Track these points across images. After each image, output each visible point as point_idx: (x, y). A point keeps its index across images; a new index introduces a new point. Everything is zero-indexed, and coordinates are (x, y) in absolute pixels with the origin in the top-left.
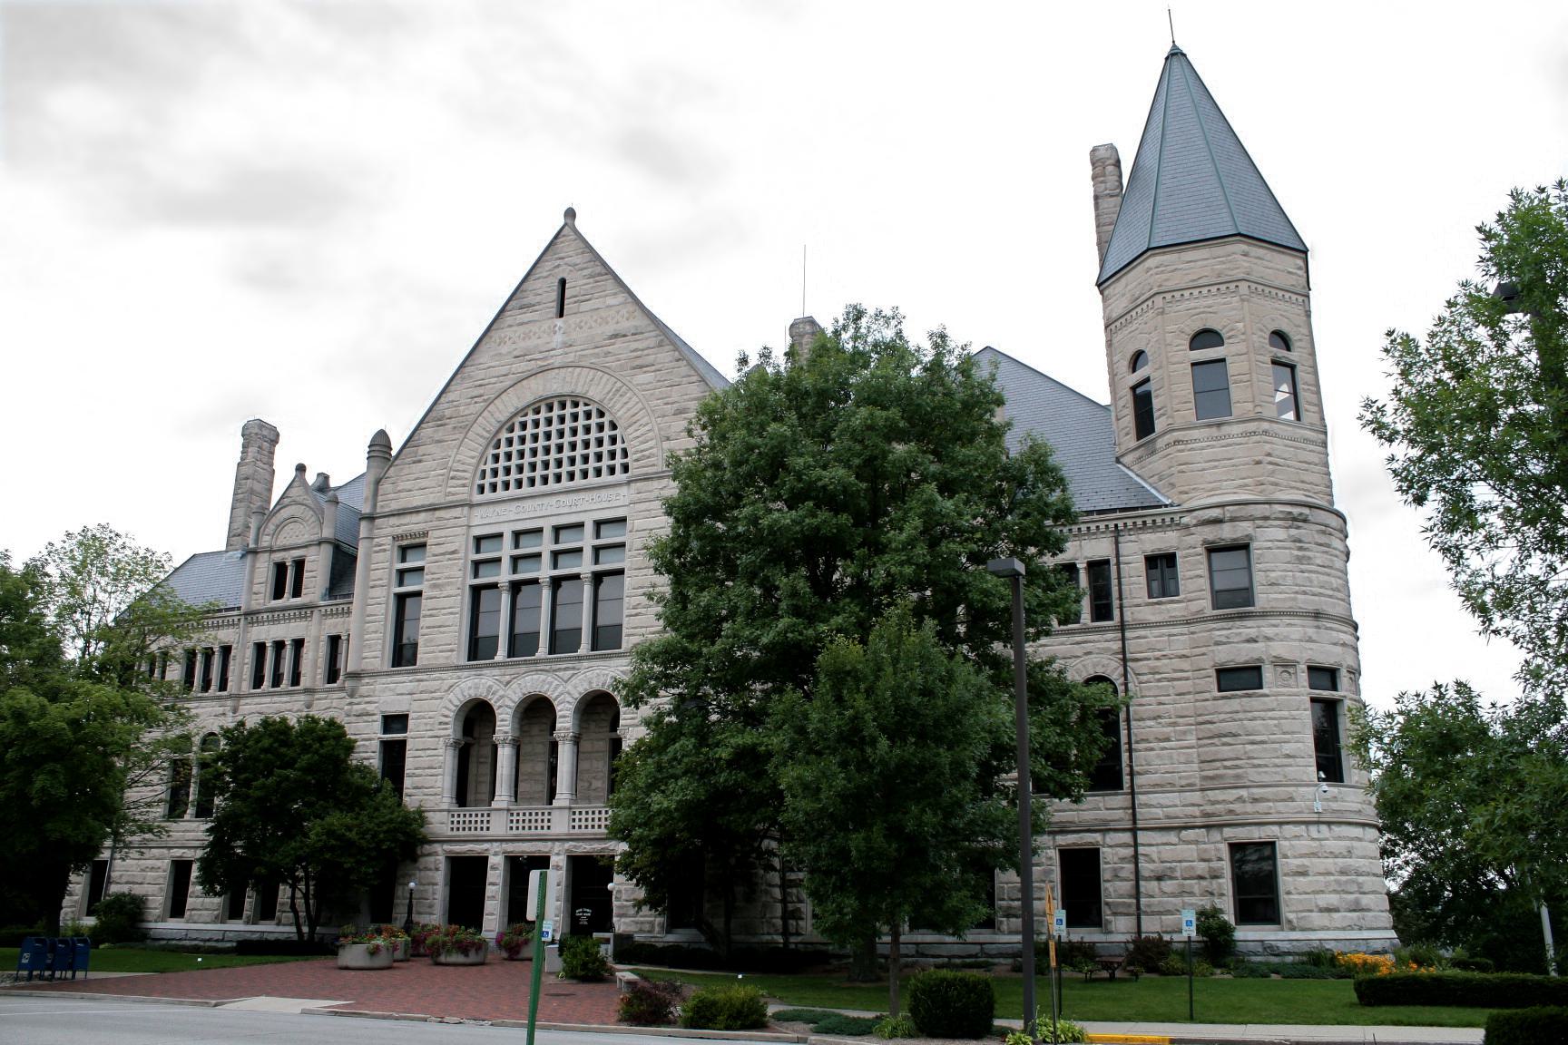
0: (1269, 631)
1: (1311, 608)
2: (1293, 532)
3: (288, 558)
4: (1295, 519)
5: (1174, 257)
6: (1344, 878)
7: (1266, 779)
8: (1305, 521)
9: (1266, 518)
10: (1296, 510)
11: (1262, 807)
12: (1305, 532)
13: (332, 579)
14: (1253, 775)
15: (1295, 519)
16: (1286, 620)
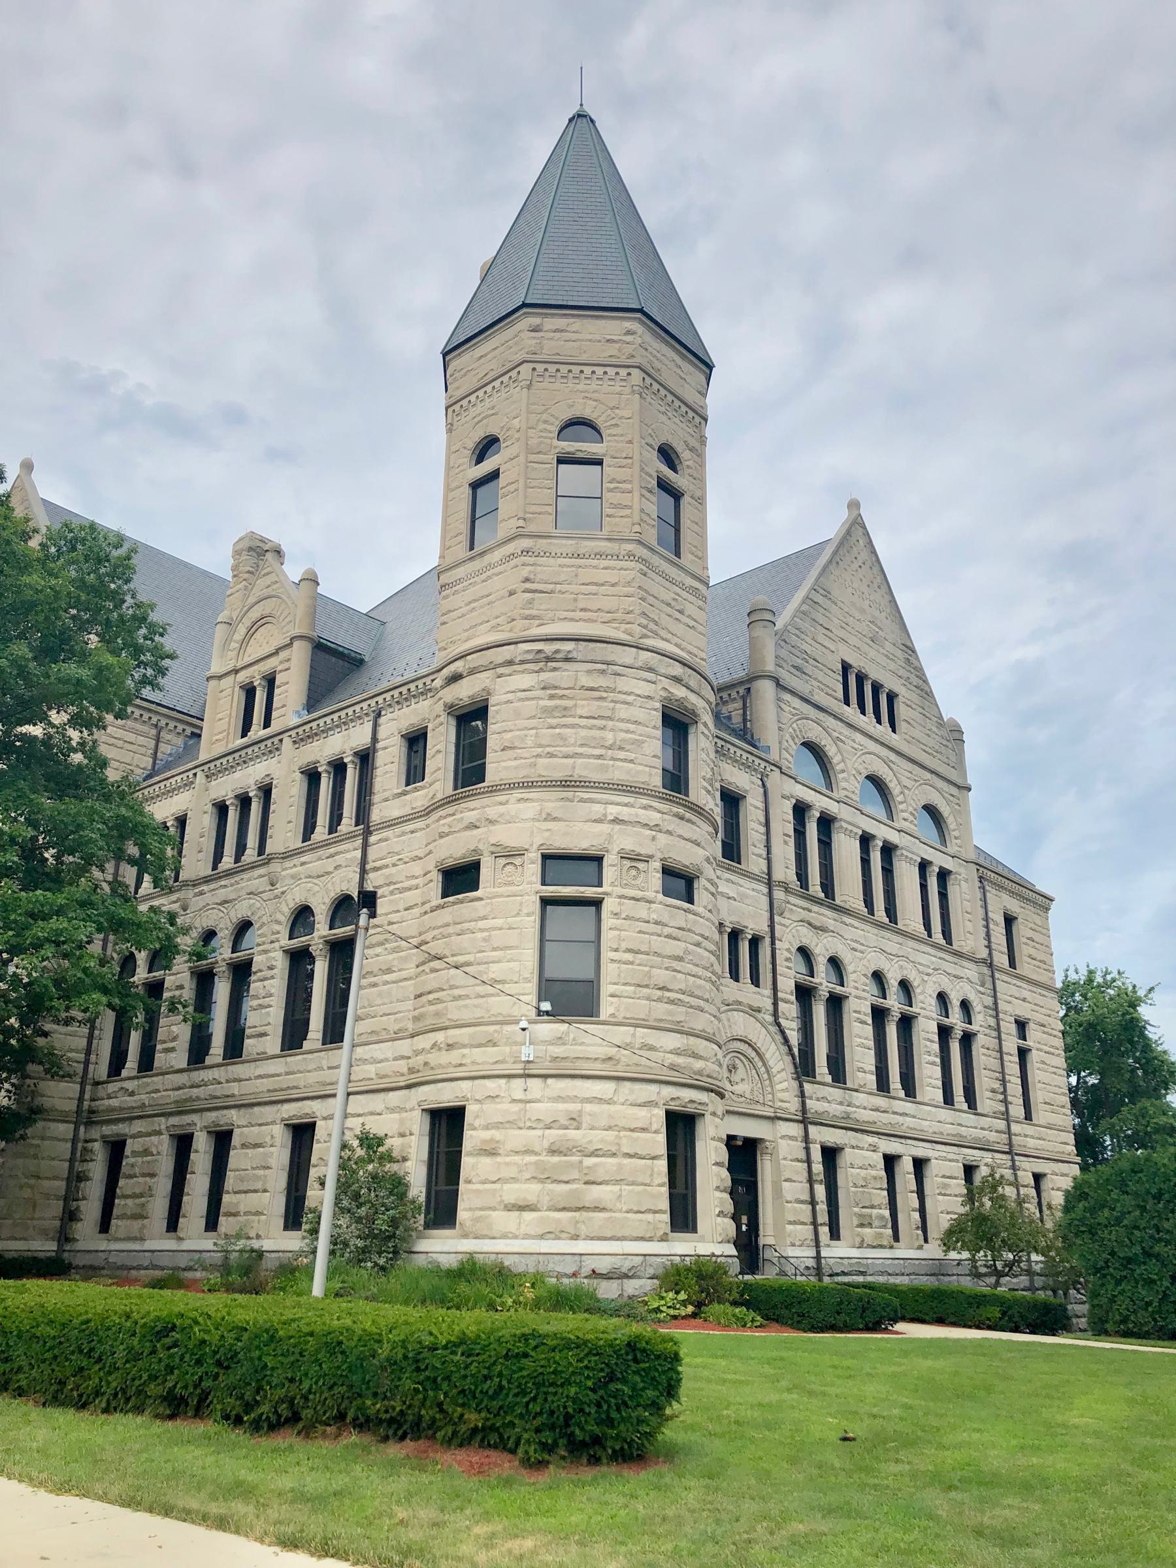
0: (492, 812)
1: (559, 775)
2: (544, 676)
3: (255, 675)
4: (548, 659)
5: (508, 334)
6: (556, 1159)
7: (466, 1016)
8: (567, 660)
9: (510, 663)
10: (549, 648)
11: (455, 1056)
12: (564, 676)
13: (309, 698)
14: (455, 1012)
15: (548, 659)
16: (517, 794)
